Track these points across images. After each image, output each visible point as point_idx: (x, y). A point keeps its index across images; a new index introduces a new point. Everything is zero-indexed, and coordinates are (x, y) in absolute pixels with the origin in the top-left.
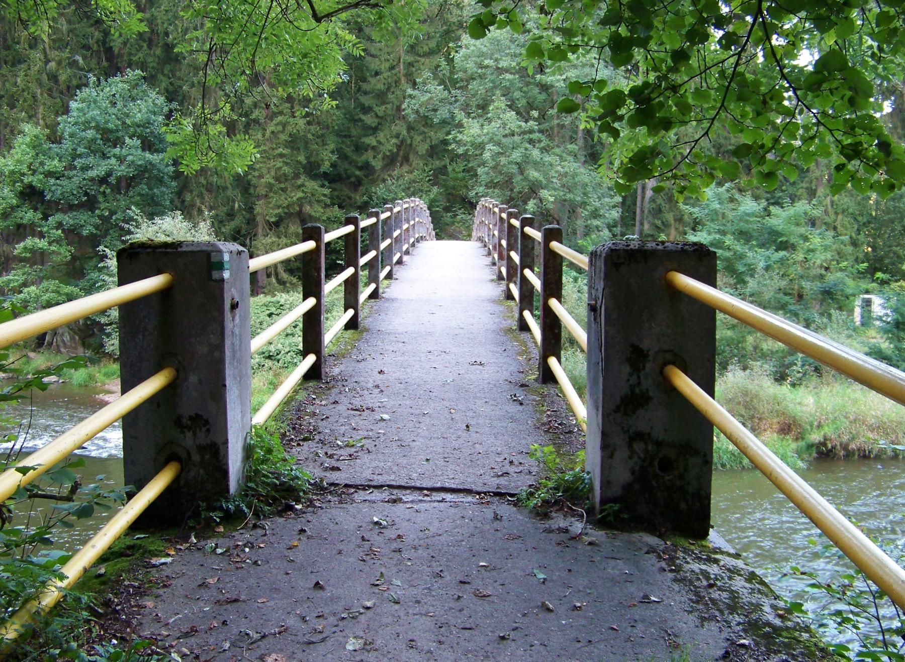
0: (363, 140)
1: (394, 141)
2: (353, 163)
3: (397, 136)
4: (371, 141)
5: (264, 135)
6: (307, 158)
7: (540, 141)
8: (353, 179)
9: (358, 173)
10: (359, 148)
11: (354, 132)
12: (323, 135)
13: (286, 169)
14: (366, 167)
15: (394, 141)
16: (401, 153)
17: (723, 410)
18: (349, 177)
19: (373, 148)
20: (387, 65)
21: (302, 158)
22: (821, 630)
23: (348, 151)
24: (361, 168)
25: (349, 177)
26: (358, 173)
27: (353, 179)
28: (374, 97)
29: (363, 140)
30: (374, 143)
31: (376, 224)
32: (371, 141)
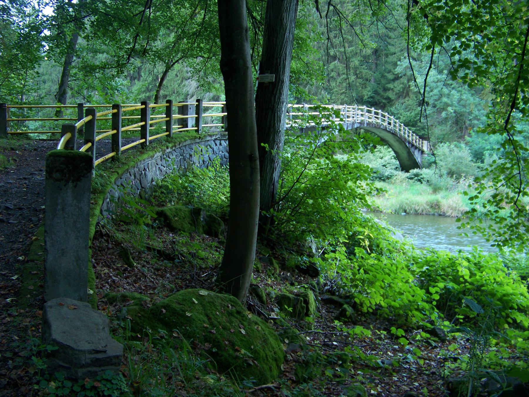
0: (387, 85)
1: (401, 86)
2: (382, 96)
3: (403, 84)
4: (390, 86)
5: (336, 84)
6: (357, 95)
7: (451, 85)
8: (382, 104)
9: (384, 101)
10: (386, 90)
11: (383, 81)
12: (365, 84)
13: (346, 99)
14: (388, 98)
15: (401, 86)
16: (405, 92)
17: (255, 248)
18: (380, 103)
19: (392, 89)
20: (399, 49)
21: (354, 94)
22: (312, 366)
23: (381, 91)
24: (385, 99)
25: (380, 103)
26: (384, 101)
27: (382, 104)
28: (392, 65)
29: (387, 85)
30: (392, 87)
31: (146, 142)
32: (390, 86)
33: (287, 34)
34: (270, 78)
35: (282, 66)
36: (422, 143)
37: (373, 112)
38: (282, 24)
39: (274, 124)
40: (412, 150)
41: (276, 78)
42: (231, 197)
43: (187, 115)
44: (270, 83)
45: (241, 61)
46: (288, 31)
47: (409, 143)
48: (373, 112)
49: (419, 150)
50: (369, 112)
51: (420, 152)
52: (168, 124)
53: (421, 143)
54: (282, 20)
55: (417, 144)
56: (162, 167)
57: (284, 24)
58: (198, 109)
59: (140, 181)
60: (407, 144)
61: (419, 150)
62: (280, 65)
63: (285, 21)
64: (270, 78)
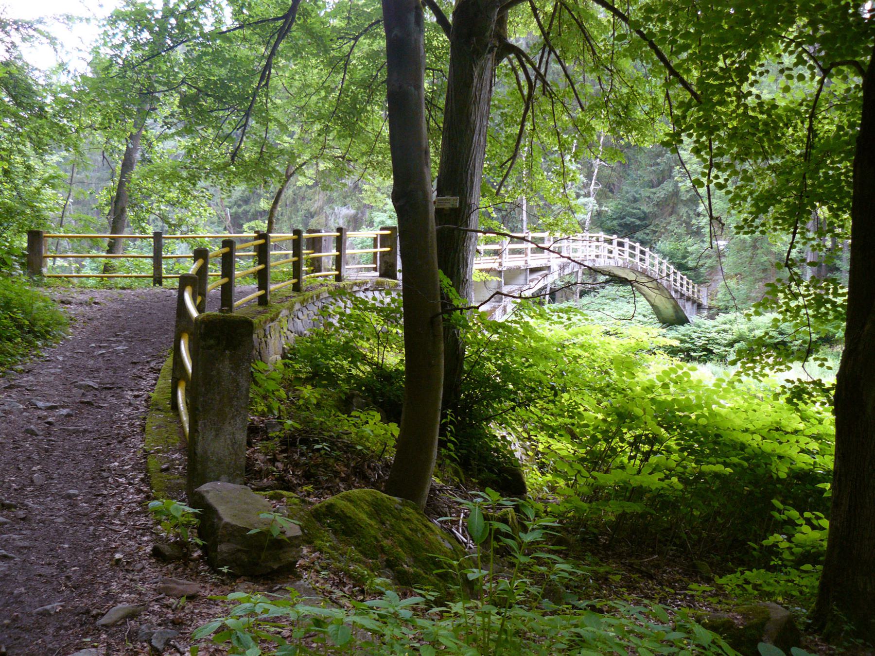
33: (476, 137)
34: (452, 202)
35: (469, 184)
36: (699, 291)
37: (615, 242)
38: (469, 122)
39: (459, 269)
40: (681, 302)
41: (461, 202)
42: (865, 97)
43: (320, 252)
44: (451, 209)
45: (420, 193)
46: (477, 132)
47: (676, 291)
48: (615, 242)
49: (694, 302)
50: (610, 242)
51: (695, 305)
52: (297, 266)
53: (696, 290)
54: (468, 116)
55: (690, 293)
56: (289, 333)
57: (472, 121)
58: (340, 243)
59: (260, 353)
60: (673, 293)
61: (694, 302)
62: (466, 183)
63: (473, 117)
64: (452, 202)
